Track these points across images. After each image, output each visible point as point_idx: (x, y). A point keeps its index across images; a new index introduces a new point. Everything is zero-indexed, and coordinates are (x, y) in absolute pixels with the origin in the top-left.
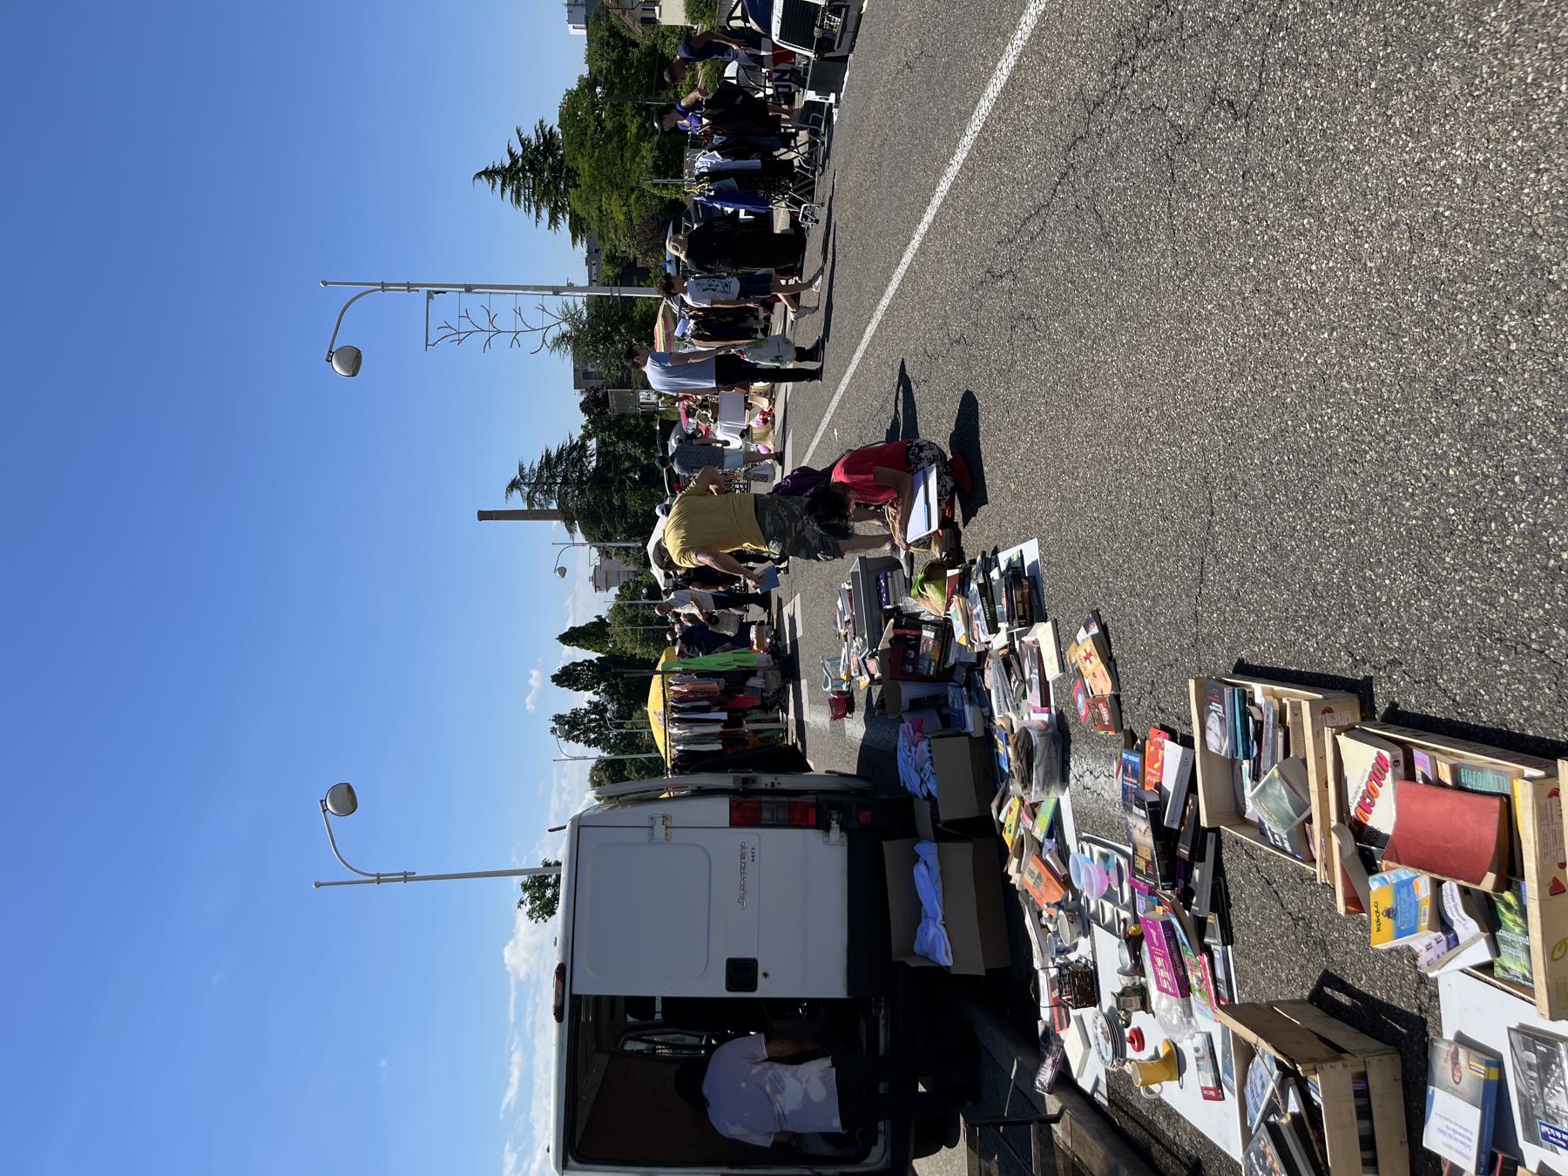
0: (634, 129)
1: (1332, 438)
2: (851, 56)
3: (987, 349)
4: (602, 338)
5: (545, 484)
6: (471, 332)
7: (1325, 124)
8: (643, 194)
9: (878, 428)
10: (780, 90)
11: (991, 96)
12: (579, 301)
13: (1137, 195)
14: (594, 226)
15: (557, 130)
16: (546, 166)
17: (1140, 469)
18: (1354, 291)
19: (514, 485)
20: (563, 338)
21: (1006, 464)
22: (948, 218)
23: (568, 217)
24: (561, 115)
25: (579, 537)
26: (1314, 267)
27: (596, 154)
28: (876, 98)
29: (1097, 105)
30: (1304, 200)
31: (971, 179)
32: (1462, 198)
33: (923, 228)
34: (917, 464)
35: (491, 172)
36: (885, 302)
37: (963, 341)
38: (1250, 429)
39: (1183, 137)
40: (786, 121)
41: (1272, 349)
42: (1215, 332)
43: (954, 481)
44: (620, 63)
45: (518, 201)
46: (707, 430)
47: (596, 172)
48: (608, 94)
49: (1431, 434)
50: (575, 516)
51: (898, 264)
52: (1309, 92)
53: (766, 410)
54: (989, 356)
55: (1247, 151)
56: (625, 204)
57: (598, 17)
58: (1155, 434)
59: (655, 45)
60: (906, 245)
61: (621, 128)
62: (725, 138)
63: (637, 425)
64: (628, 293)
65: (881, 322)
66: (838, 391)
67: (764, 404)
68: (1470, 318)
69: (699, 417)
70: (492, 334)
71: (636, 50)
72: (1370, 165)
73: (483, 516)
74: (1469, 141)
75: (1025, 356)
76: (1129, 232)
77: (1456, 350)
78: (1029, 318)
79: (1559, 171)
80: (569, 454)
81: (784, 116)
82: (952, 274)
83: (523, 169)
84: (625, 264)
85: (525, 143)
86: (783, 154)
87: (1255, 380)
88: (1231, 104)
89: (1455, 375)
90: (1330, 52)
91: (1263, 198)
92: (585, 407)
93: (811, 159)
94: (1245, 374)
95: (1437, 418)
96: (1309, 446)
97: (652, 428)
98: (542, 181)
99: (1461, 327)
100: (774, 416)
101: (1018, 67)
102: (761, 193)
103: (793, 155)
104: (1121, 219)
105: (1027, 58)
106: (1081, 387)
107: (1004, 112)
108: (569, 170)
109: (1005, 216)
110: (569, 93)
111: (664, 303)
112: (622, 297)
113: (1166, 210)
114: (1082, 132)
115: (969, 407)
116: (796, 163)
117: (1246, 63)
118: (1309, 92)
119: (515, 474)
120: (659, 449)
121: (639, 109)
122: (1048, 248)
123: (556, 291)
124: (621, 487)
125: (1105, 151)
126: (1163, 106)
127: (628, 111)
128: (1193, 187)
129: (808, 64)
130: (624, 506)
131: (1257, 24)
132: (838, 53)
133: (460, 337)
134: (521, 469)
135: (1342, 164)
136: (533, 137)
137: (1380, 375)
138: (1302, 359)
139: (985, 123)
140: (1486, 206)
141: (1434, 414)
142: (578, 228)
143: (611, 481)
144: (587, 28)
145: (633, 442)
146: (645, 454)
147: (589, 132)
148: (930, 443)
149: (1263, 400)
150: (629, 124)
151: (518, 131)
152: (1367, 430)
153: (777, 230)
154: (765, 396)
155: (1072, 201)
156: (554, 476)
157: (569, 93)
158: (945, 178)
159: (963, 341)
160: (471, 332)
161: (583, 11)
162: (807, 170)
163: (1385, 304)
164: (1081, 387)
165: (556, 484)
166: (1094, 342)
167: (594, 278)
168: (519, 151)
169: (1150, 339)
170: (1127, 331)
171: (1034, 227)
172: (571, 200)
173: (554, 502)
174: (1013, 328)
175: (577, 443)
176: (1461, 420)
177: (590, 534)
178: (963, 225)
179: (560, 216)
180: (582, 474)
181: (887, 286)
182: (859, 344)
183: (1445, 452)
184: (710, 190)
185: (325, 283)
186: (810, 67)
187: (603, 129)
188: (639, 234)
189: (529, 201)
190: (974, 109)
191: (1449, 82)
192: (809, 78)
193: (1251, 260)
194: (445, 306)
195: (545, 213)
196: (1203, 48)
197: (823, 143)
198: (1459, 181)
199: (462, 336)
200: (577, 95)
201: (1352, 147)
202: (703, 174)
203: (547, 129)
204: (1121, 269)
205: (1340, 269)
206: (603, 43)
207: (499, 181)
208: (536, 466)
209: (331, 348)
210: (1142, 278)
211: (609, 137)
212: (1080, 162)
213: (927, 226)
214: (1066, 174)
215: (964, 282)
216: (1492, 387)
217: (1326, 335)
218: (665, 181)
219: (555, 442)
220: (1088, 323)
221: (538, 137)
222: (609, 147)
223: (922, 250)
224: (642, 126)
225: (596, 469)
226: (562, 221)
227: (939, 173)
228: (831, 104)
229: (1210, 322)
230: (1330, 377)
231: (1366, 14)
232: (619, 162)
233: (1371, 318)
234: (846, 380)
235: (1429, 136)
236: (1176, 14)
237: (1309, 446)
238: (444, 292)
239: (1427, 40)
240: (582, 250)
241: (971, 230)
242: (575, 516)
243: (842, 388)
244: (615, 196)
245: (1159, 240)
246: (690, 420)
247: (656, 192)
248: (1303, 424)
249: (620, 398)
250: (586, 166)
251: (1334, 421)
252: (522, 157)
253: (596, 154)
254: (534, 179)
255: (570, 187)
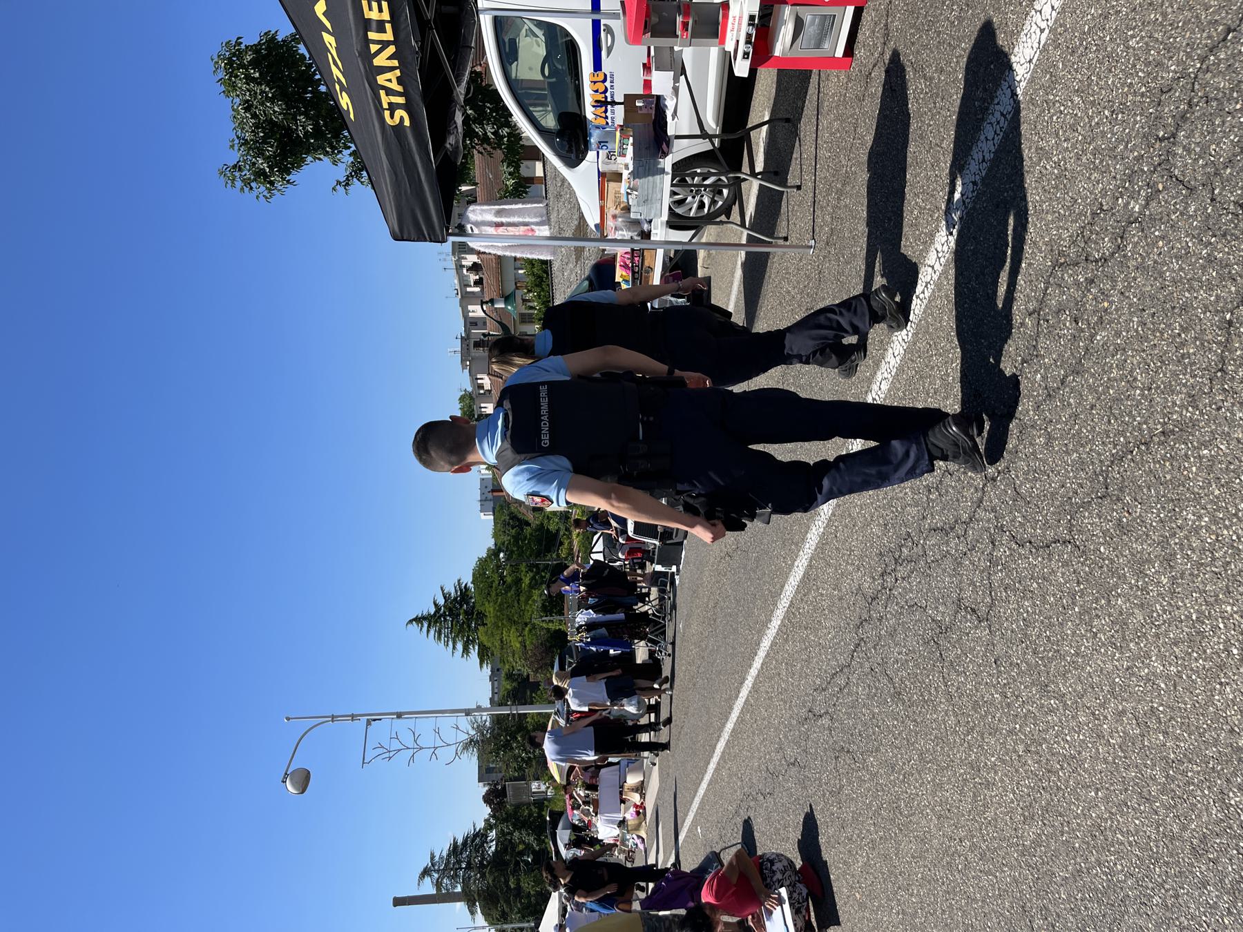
0: (527, 581)
1: (1121, 881)
2: (685, 542)
3: (817, 773)
4: (503, 746)
5: (452, 869)
6: (399, 750)
7: (1048, 632)
8: (534, 627)
9: (735, 830)
10: (635, 561)
11: (793, 583)
12: (486, 717)
13: (917, 666)
14: (497, 653)
15: (471, 585)
16: (462, 611)
17: (965, 892)
18: (1105, 761)
19: (426, 872)
20: (471, 742)
21: (849, 874)
22: (772, 667)
23: (477, 647)
24: (474, 575)
25: (480, 919)
26: (1068, 738)
27: (499, 600)
28: (707, 573)
29: (873, 599)
30: (1046, 686)
31: (786, 640)
32: (1169, 698)
33: (753, 672)
34: (772, 877)
35: (420, 618)
36: (730, 726)
37: (797, 764)
38: (1051, 867)
39: (944, 630)
40: (640, 582)
41: (1053, 800)
42: (1002, 781)
43: (807, 888)
44: (516, 538)
45: (439, 638)
46: (589, 821)
47: (498, 614)
48: (508, 559)
49: (1199, 885)
50: (477, 898)
51: (737, 697)
52: (1029, 609)
53: (639, 804)
54: (820, 779)
55: (993, 645)
56: (520, 635)
57: (502, 507)
58: (971, 862)
59: (542, 524)
60: (742, 683)
61: (518, 581)
62: (597, 600)
63: (530, 815)
64: (523, 710)
65: (728, 741)
66: (698, 794)
67: (636, 798)
68: (1202, 792)
69: (583, 812)
70: (415, 750)
71: (528, 528)
72: (1091, 666)
73: (398, 902)
74: (1161, 657)
75: (850, 782)
76: (916, 693)
77: (1199, 816)
78: (848, 752)
79: (1237, 685)
80: (473, 841)
81: (639, 578)
82: (781, 710)
83: (444, 615)
84: (519, 680)
85: (446, 597)
86: (641, 608)
87: (1045, 824)
88: (973, 610)
89: (1205, 837)
90: (1038, 583)
91: (1015, 681)
92: (487, 799)
93: (661, 608)
94: (1035, 818)
95: (1201, 872)
96: (1103, 887)
97: (542, 817)
98: (458, 622)
99: (1198, 798)
100: (645, 809)
101: (810, 566)
102: (626, 637)
103: (647, 608)
104: (906, 682)
105: (816, 561)
106: (901, 813)
107: (805, 595)
108: (479, 613)
109: (817, 670)
110: (480, 560)
111: (552, 718)
112: (519, 714)
113: (941, 679)
114: (865, 616)
115: (810, 826)
116: (650, 612)
117: (978, 584)
118: (1029, 609)
119: (427, 862)
120: (549, 837)
121: (530, 568)
122: (855, 698)
123: (468, 713)
124: (516, 871)
125: (886, 632)
126: (924, 606)
127: (523, 569)
128: (959, 666)
129: (655, 548)
130: (518, 888)
131: (979, 559)
132: (676, 540)
133: (390, 755)
134: (432, 857)
135: (1069, 663)
136: (453, 591)
137: (1145, 832)
138: (1079, 812)
139: (791, 602)
140: (1189, 706)
141: (1198, 869)
142: (484, 655)
143: (507, 864)
144: (494, 515)
145: (526, 830)
146: (537, 840)
147: (494, 585)
148: (778, 855)
149: (1056, 842)
150: (523, 578)
151: (442, 588)
152: (1147, 878)
153: (639, 661)
154: (637, 792)
155: (867, 665)
156: (459, 862)
157: (480, 560)
158: (766, 638)
159: (797, 764)
160: (399, 750)
161: (491, 504)
162: (659, 617)
163: (1133, 774)
164: (901, 813)
165: (461, 869)
166: (905, 778)
167: (496, 691)
168: (441, 601)
169: (950, 779)
170: (930, 771)
171: (841, 681)
172: (479, 635)
173: (459, 886)
174: (837, 758)
175: (480, 831)
176: (1222, 876)
177: (489, 915)
178: (784, 674)
179: (471, 647)
180: (483, 858)
181: (730, 713)
182: (712, 757)
183: (1216, 903)
184: (587, 638)
185: (288, 719)
186: (657, 550)
187: (504, 582)
188: (531, 657)
189: (448, 638)
190: (782, 591)
191: (1133, 613)
192: (656, 557)
193: (1017, 726)
194: (381, 731)
195: (460, 646)
196: (944, 570)
197: (670, 598)
198: (1163, 685)
199: (392, 754)
200: (486, 561)
201: (1073, 652)
202: (581, 626)
203: (463, 585)
204: (915, 721)
205: (1090, 742)
206: (505, 524)
207: (426, 625)
208: (445, 854)
209: (287, 770)
210: (933, 729)
211: (509, 587)
212: (868, 637)
213: (757, 672)
214: (859, 645)
215: (791, 717)
216: (1237, 850)
217: (1093, 794)
218: (552, 618)
219: (461, 832)
220: (897, 761)
221: (456, 591)
222: (509, 595)
223: (755, 689)
224: (533, 578)
225: (496, 852)
226: (472, 651)
227: (761, 633)
228: (673, 573)
229: (996, 773)
230: (1106, 829)
231: (1059, 561)
232: (516, 604)
233: (1125, 784)
234: (704, 785)
235: (1130, 650)
236: (920, 546)
237: (1103, 887)
238: (380, 720)
239: (1109, 583)
240: (487, 671)
241: (792, 678)
242: (477, 898)
243: (701, 791)
244: (513, 630)
245: (941, 702)
246: (575, 812)
247: (544, 625)
248: (1094, 867)
249: (515, 789)
250: (491, 609)
251: (1119, 867)
252: (444, 606)
253: (499, 600)
254: (452, 622)
255: (479, 625)
